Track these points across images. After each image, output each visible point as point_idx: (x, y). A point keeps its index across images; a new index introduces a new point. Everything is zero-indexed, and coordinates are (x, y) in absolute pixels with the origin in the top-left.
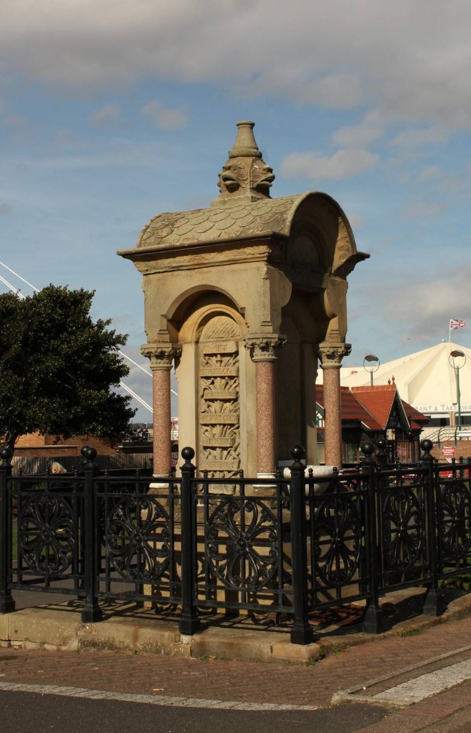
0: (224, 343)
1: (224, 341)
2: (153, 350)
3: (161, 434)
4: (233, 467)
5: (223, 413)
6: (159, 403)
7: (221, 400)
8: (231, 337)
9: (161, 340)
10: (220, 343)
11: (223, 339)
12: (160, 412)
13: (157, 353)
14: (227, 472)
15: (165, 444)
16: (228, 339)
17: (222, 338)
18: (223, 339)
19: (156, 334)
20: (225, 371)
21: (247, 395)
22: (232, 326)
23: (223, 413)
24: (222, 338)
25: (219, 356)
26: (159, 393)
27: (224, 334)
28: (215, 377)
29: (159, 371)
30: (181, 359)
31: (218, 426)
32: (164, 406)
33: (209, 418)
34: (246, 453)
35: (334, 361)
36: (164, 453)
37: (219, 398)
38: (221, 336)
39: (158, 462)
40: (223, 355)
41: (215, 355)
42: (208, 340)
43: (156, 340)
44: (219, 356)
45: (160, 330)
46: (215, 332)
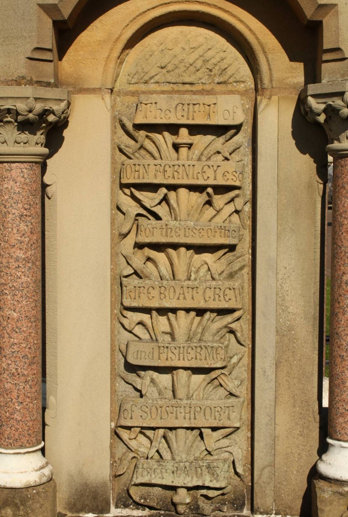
0: (208, 99)
1: (194, 93)
2: (21, 106)
3: (26, 339)
4: (229, 418)
5: (203, 279)
6: (20, 254)
7: (188, 247)
8: (219, 83)
9: (35, 79)
10: (195, 97)
11: (194, 88)
12: (24, 279)
13: (31, 115)
14: (210, 430)
15: (34, 367)
16: (208, 87)
17: (191, 84)
18: (194, 88)
19: (23, 60)
20: (210, 173)
21: (279, 237)
22: (222, 55)
23: (203, 279)
24: (191, 84)
25: (184, 132)
26: (22, 226)
27: (199, 74)
28: (173, 188)
29: (22, 166)
30: (66, 133)
31: (181, 313)
32: (33, 263)
33: (155, 293)
34: (273, 384)
35: (34, 138)
36: (34, 390)
37: (182, 240)
38: (187, 79)
39: (17, 416)
40: (195, 129)
41: (174, 129)
42: (143, 87)
43: (23, 78)
44: (184, 132)
45: (37, 49)
46: (170, 67)
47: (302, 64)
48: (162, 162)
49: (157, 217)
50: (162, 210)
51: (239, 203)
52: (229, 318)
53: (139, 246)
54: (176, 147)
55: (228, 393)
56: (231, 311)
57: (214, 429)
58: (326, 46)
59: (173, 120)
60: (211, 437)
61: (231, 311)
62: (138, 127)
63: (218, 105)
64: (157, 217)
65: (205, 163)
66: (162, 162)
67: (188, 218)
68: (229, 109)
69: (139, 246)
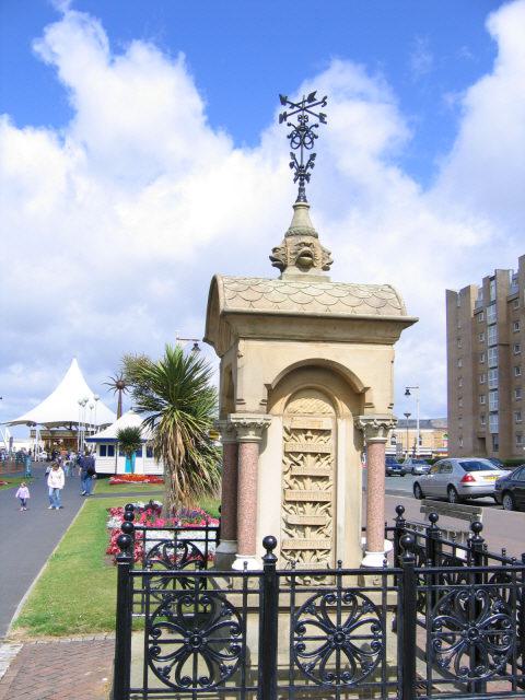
0: (318, 419)
28: (305, 454)
30: (269, 430)
40: (314, 431)
41: (305, 431)
47: (242, 344)
48: (300, 443)
49: (299, 465)
50: (301, 462)
51: (330, 460)
52: (325, 506)
53: (292, 477)
54: (306, 438)
55: (339, 421)
56: (327, 503)
57: (321, 550)
58: (238, 398)
59: (306, 427)
60: (319, 554)
61: (327, 503)
62: (293, 430)
63: (280, 473)
64: (299, 465)
65: (317, 444)
66: (300, 443)
67: (310, 466)
68: (327, 424)
69: (292, 477)
